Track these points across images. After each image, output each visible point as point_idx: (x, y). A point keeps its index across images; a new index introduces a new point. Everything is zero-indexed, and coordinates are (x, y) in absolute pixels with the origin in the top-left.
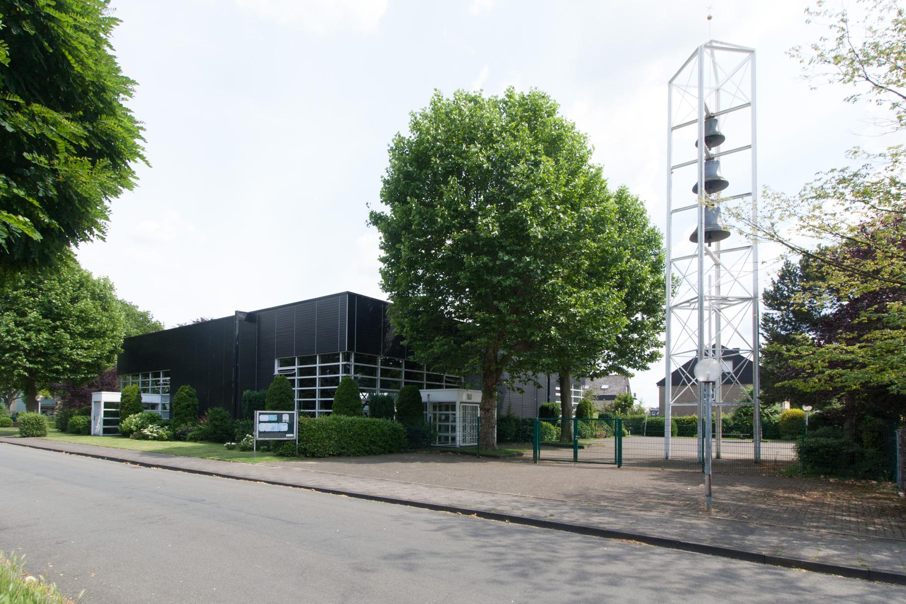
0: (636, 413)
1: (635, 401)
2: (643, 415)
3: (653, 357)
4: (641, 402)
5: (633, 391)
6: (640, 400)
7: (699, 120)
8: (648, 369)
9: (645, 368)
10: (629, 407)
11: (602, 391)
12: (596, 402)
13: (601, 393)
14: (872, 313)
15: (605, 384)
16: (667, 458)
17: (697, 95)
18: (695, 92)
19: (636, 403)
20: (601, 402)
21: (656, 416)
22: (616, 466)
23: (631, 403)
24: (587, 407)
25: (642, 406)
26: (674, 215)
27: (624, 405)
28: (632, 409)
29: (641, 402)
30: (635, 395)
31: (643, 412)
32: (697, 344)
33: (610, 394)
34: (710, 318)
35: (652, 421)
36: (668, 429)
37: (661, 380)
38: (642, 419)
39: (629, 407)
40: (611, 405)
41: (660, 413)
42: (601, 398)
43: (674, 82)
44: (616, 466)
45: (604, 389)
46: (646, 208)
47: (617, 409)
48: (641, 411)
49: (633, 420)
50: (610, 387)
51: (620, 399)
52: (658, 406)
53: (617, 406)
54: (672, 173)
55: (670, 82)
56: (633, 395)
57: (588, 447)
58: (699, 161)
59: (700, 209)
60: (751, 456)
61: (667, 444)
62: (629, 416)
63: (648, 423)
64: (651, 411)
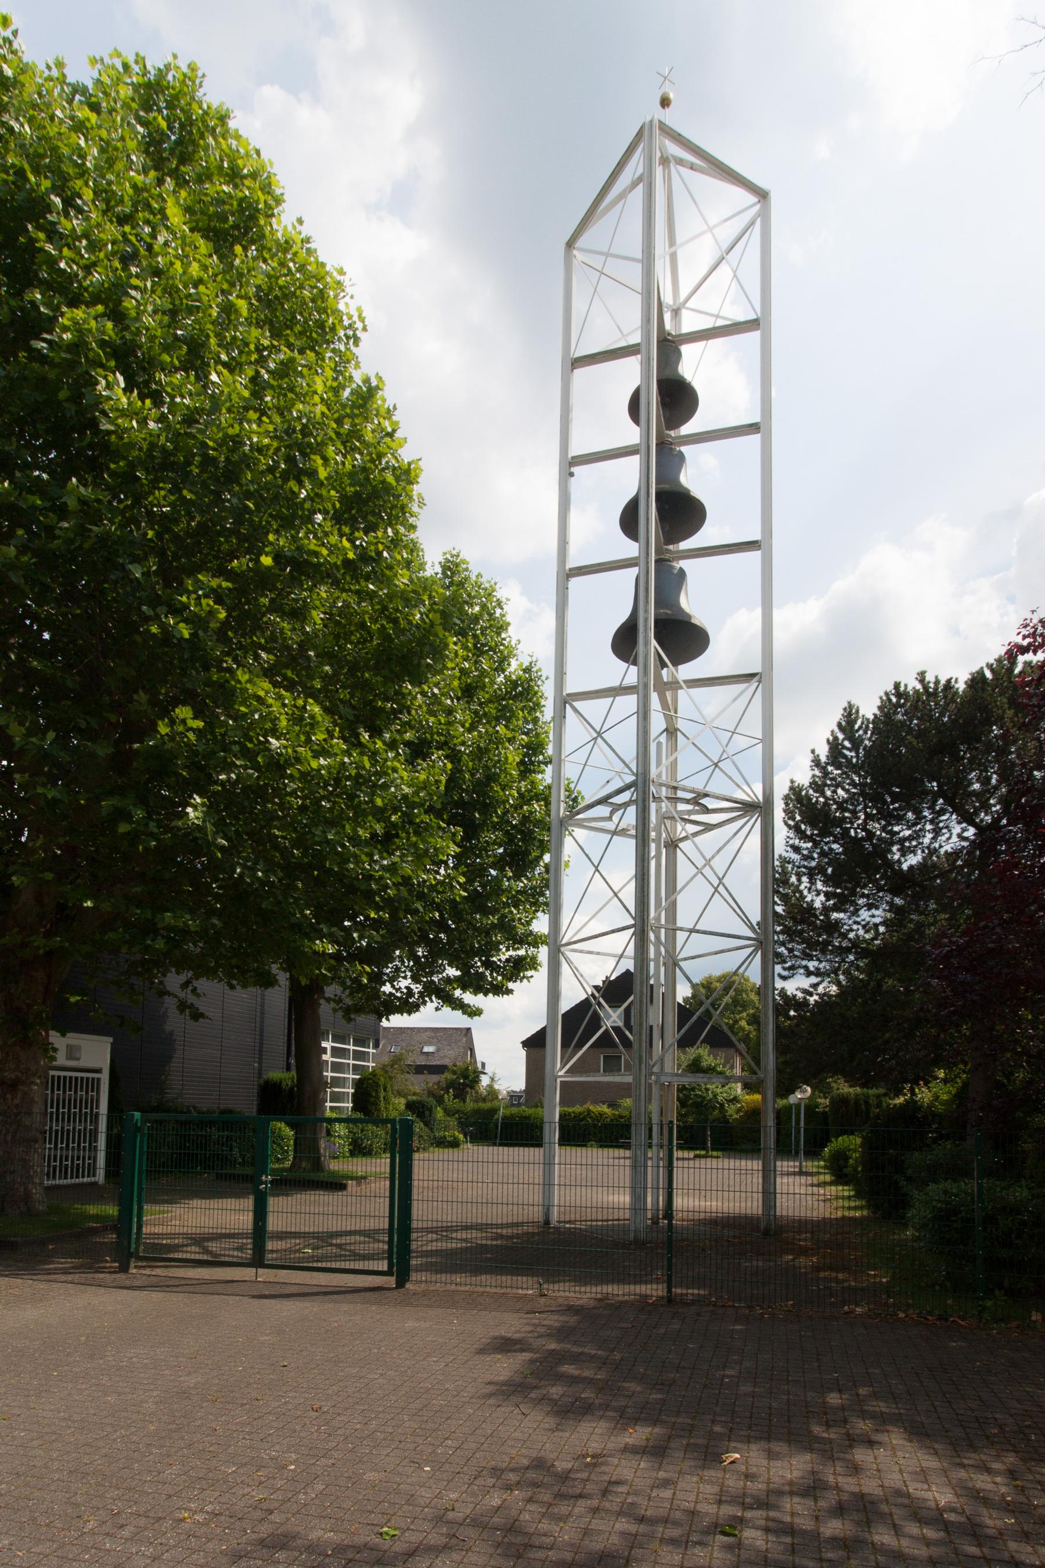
0: (484, 1100)
1: (483, 1078)
2: (496, 1103)
3: (518, 968)
4: (492, 1079)
5: (480, 1056)
6: (491, 1074)
7: (643, 349)
8: (509, 992)
9: (499, 990)
10: (472, 1088)
11: (423, 1057)
12: (412, 1077)
13: (421, 1061)
14: (115, 1272)
15: (430, 1044)
16: (547, 1222)
17: (638, 285)
18: (634, 275)
19: (485, 1081)
20: (421, 1077)
21: (519, 1105)
22: (391, 1281)
23: (476, 1080)
24: (378, 1085)
25: (496, 1087)
26: (574, 583)
27: (463, 1084)
28: (477, 1092)
29: (492, 1079)
30: (483, 1065)
31: (497, 1098)
32: (746, 685)
33: (438, 1063)
34: (658, 856)
35: (512, 1115)
36: (553, 1133)
37: (534, 1032)
38: (494, 1111)
39: (472, 1088)
40: (438, 1083)
41: (526, 1101)
42: (419, 1069)
43: (580, 243)
44: (391, 1281)
45: (427, 1053)
46: (508, 618)
47: (448, 1092)
48: (492, 1093)
49: (477, 1112)
50: (438, 1050)
51: (454, 1072)
52: (523, 1087)
53: (451, 1085)
54: (572, 475)
55: (570, 244)
56: (479, 1066)
57: (359, 1184)
58: (643, 450)
59: (643, 545)
60: (752, 1205)
61: (548, 1164)
62: (470, 1105)
63: (504, 1118)
64: (512, 1096)
